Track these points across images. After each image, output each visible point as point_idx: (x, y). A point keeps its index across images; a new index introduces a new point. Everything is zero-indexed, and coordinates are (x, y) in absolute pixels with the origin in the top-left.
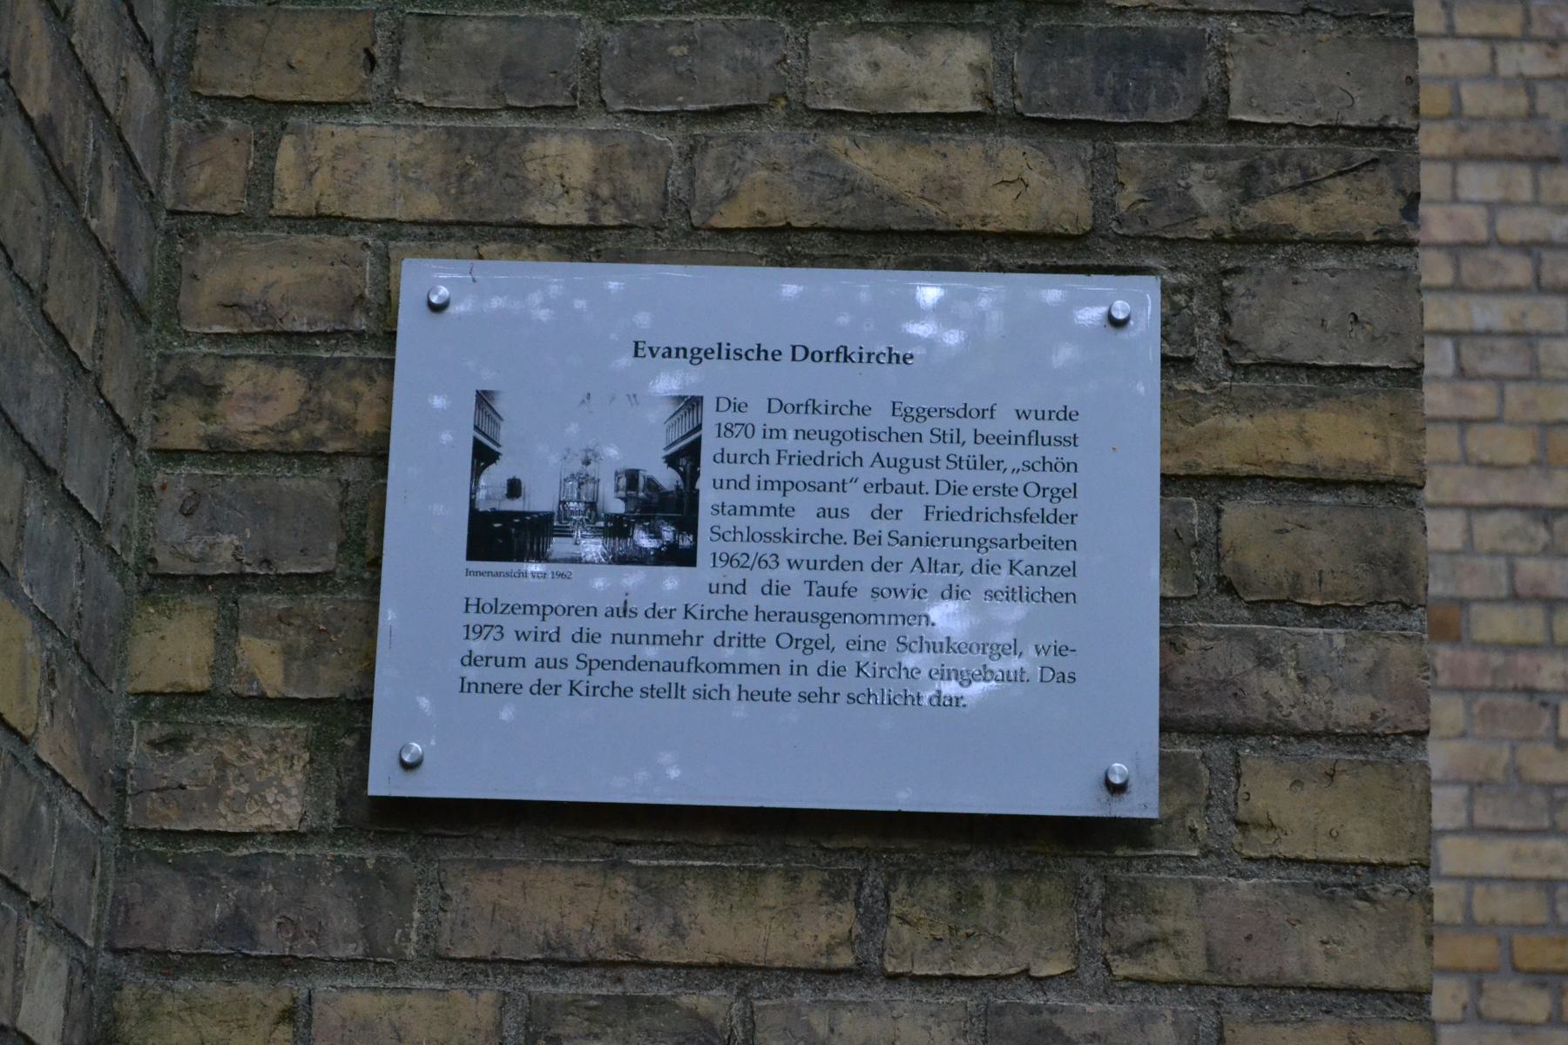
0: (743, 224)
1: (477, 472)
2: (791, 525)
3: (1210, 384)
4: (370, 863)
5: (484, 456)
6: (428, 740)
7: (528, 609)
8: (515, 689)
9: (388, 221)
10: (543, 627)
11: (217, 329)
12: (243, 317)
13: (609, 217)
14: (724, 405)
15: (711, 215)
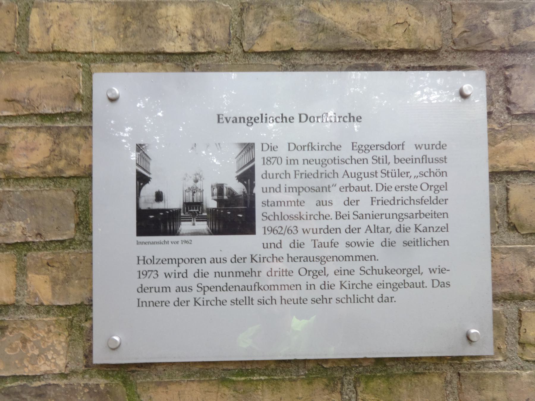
0: (269, 49)
1: (139, 189)
2: (303, 210)
3: (501, 125)
4: (102, 387)
5: (142, 179)
6: (126, 331)
7: (170, 261)
8: (166, 303)
9: (89, 53)
10: (178, 270)
11: (6, 113)
12: (18, 106)
13: (202, 47)
14: (265, 147)
15: (253, 45)
